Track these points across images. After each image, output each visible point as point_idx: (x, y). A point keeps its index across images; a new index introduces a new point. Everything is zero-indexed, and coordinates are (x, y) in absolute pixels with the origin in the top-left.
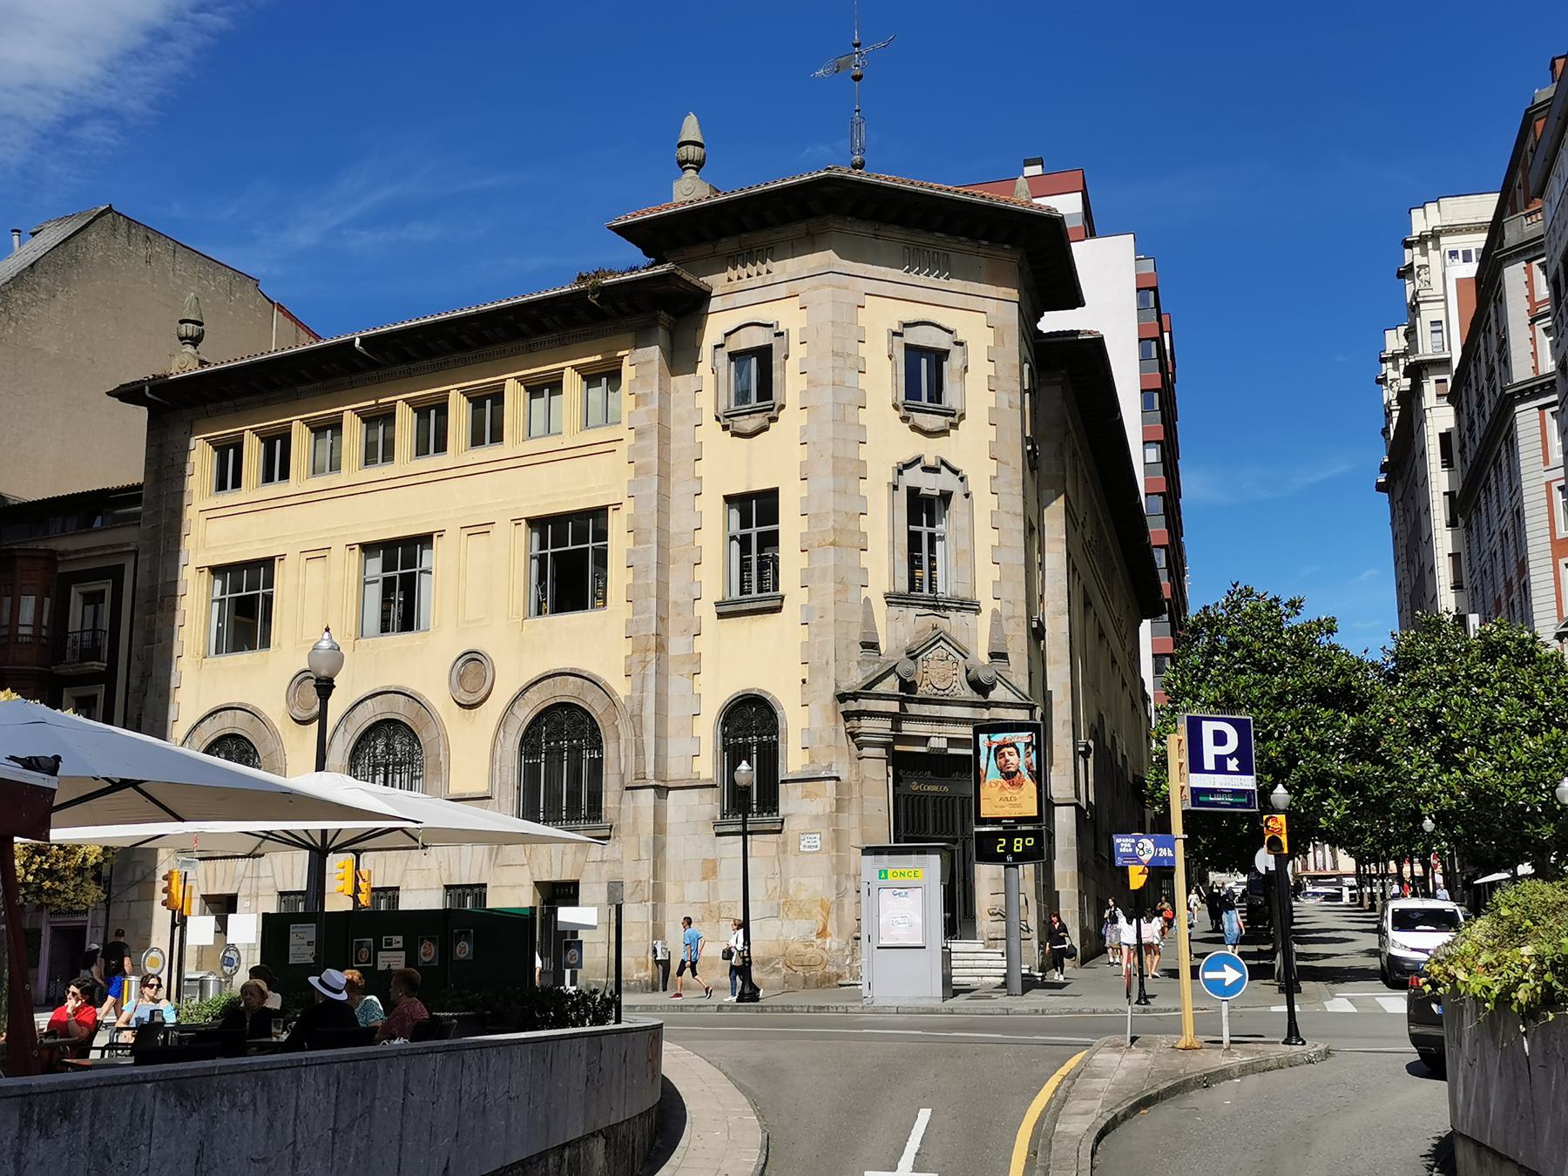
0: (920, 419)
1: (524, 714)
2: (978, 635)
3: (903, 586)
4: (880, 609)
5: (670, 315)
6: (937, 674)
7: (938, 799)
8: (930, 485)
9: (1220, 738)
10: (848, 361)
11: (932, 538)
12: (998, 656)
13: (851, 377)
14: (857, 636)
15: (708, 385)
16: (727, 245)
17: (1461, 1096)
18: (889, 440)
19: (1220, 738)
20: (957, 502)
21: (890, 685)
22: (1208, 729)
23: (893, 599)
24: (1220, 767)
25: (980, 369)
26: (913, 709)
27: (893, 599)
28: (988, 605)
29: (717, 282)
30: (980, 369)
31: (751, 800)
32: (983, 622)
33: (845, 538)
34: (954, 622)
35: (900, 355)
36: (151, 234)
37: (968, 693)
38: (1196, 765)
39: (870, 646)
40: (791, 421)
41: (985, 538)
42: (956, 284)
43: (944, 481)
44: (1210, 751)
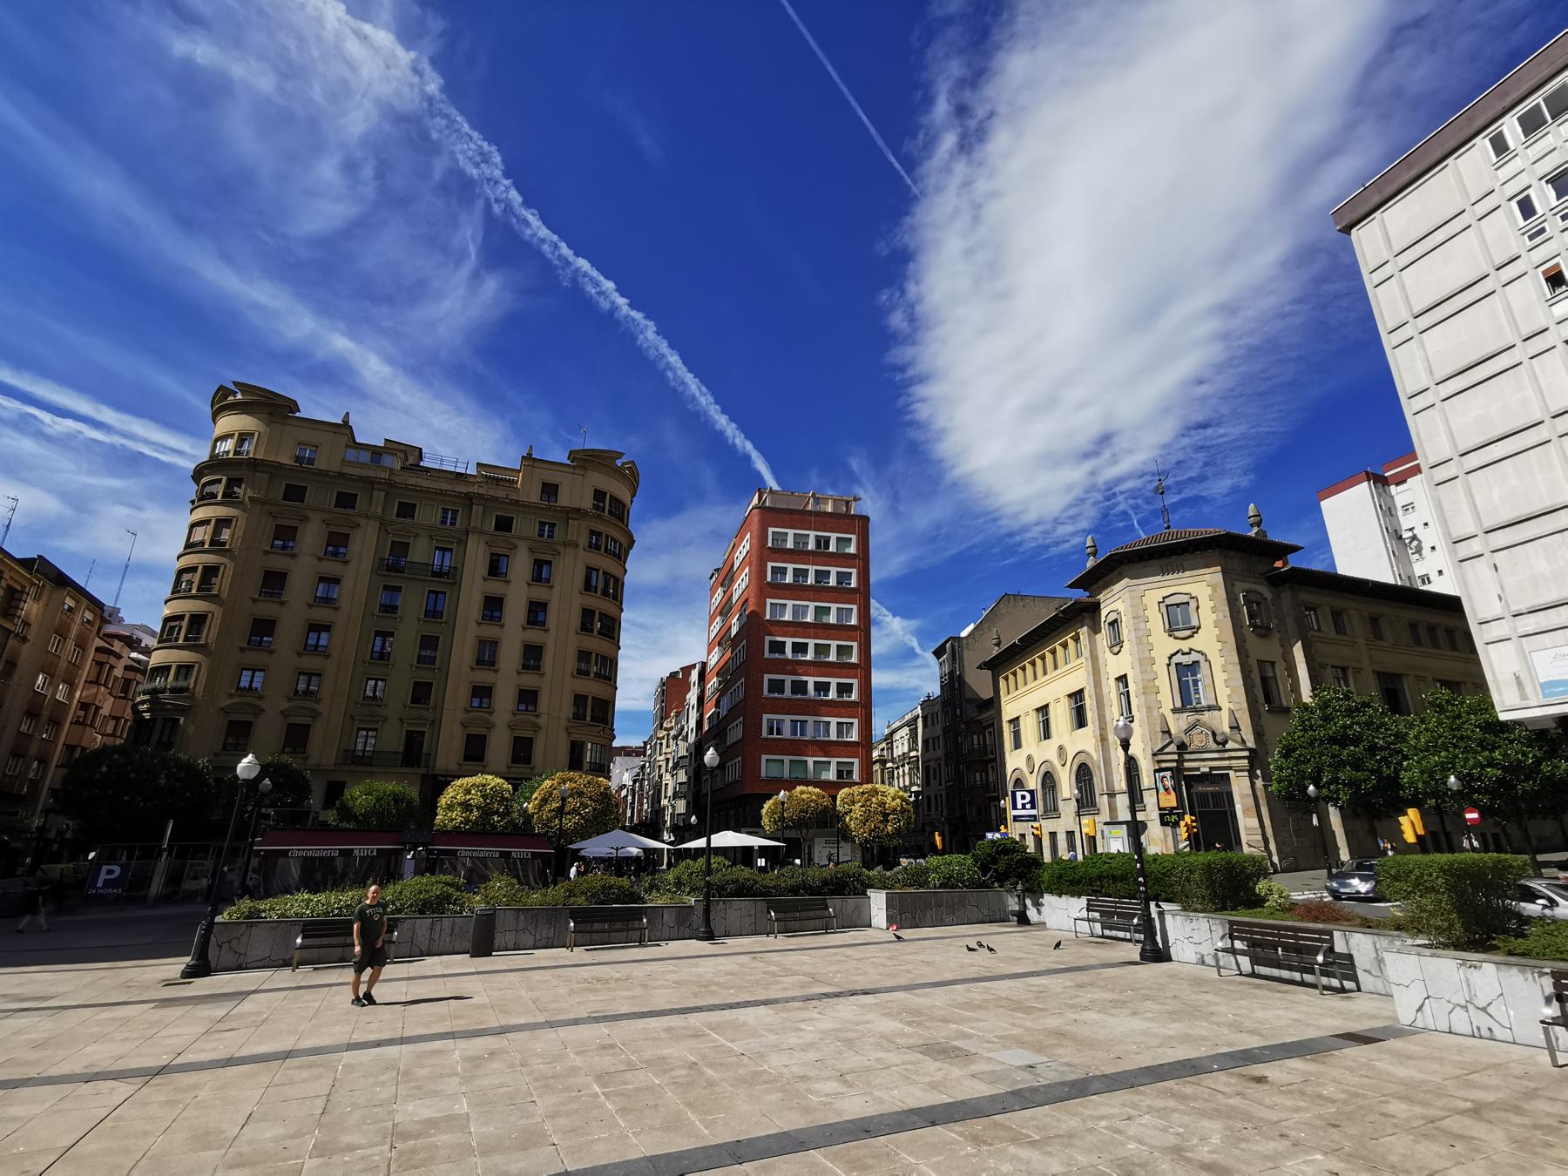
0: (1177, 634)
1: (1075, 767)
2: (1223, 723)
3: (1179, 704)
4: (1170, 717)
5: (1086, 613)
6: (1197, 740)
7: (1213, 794)
8: (1186, 660)
9: (1023, 797)
10: (1140, 618)
11: (1196, 683)
12: (1235, 728)
13: (1142, 625)
14: (1158, 729)
15: (1103, 639)
16: (1101, 583)
17: (1121, 934)
18: (1164, 645)
19: (1023, 797)
20: (1203, 665)
21: (1173, 748)
22: (1019, 794)
23: (1175, 711)
24: (1024, 806)
25: (1206, 605)
26: (1187, 757)
27: (1175, 711)
28: (1224, 702)
29: (1101, 597)
30: (1206, 605)
31: (1086, 802)
32: (1225, 714)
33: (1150, 689)
34: (1206, 717)
35: (1164, 610)
36: (1023, 597)
37: (1214, 746)
38: (1015, 808)
39: (1168, 732)
40: (1126, 645)
41: (1220, 677)
42: (1187, 573)
43: (1194, 657)
44: (1020, 802)
